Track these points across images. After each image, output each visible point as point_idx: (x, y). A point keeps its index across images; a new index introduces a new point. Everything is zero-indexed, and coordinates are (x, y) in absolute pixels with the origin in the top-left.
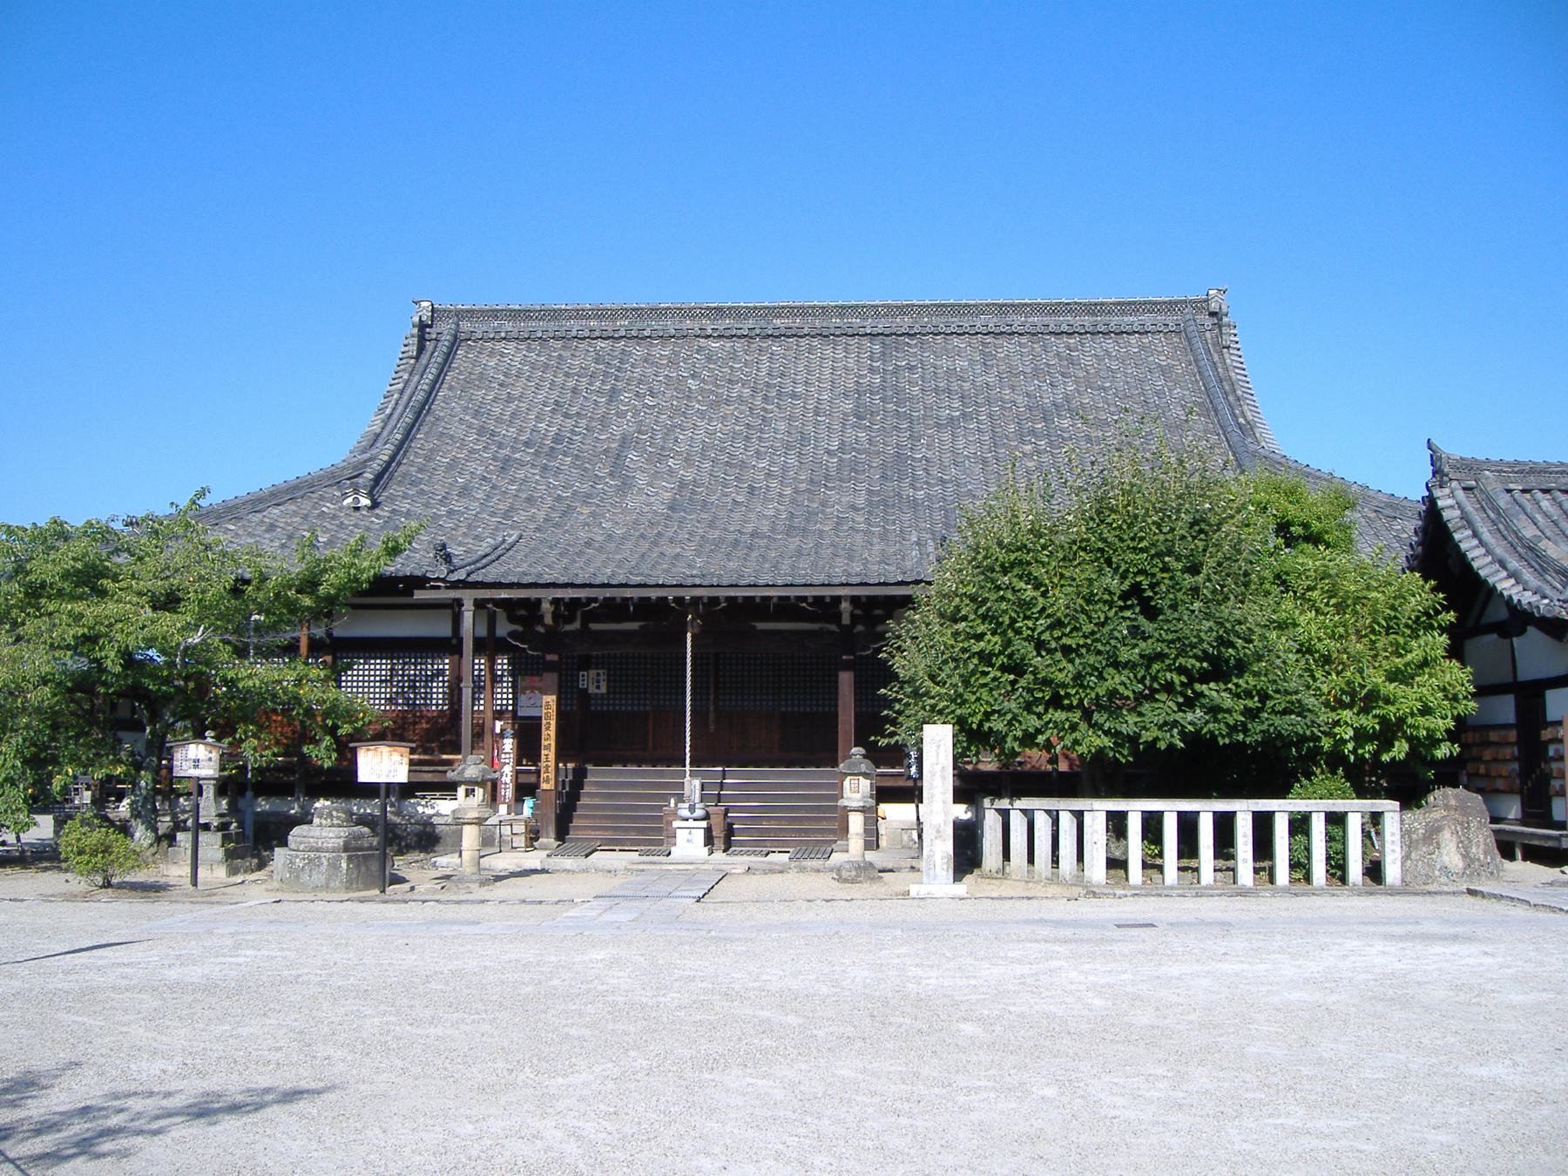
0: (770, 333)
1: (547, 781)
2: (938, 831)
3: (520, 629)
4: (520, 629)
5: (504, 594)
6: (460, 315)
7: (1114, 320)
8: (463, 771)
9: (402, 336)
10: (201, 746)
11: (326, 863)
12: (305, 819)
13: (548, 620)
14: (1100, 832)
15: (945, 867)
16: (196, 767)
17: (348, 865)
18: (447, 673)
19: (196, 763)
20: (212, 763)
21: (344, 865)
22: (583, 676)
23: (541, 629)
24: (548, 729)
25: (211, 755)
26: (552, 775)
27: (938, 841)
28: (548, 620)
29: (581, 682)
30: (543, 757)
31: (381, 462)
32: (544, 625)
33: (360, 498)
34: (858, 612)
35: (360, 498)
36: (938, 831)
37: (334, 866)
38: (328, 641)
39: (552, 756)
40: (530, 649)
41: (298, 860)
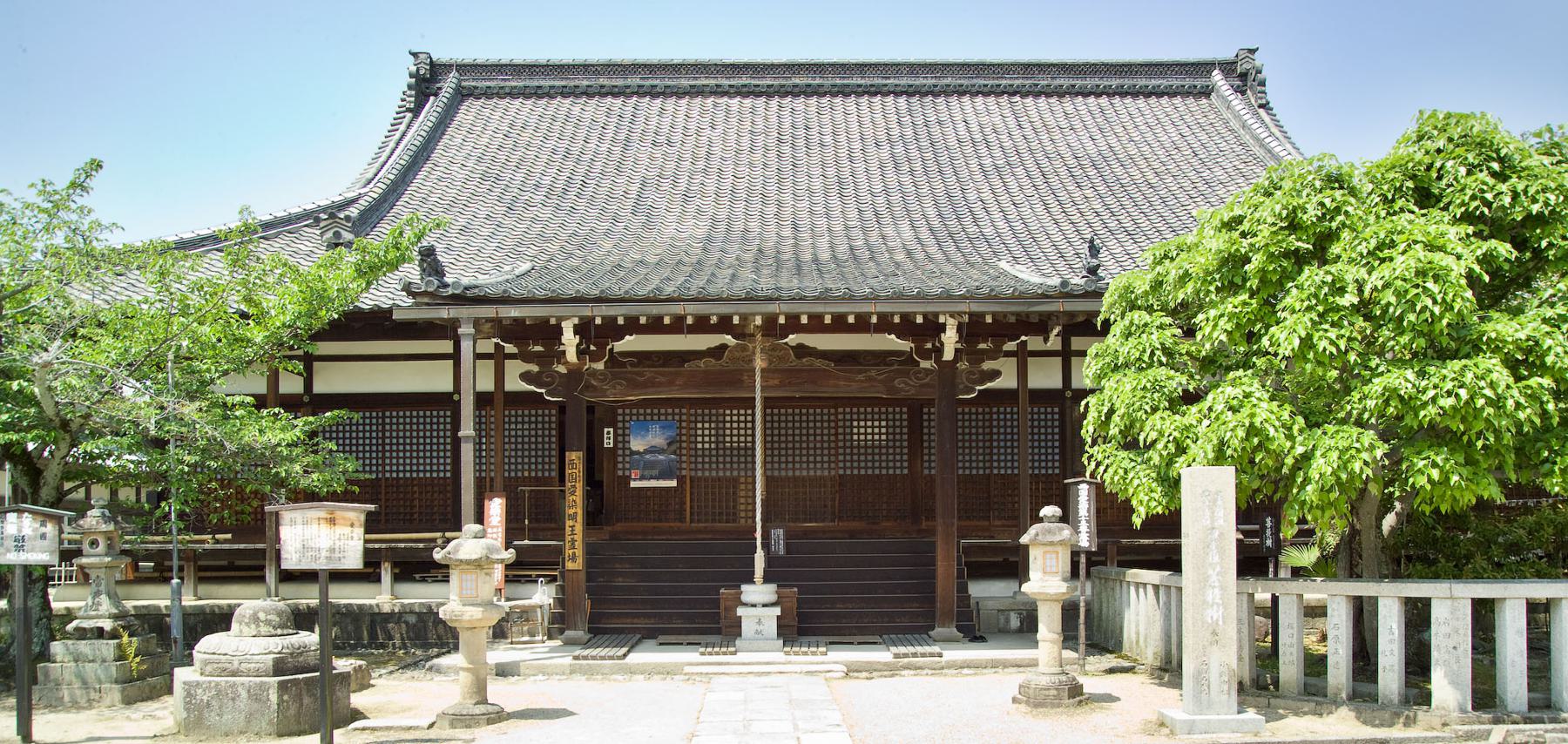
0: (789, 90)
1: (573, 558)
2: (1214, 633)
3: (535, 368)
4: (535, 368)
5: (514, 312)
6: (463, 68)
7: (1141, 82)
8: (456, 550)
9: (397, 84)
10: (27, 516)
11: (244, 694)
12: (220, 621)
13: (571, 356)
14: (1461, 631)
15: (1226, 687)
16: (19, 548)
17: (280, 697)
18: (449, 488)
19: (20, 543)
20: (45, 543)
21: (274, 697)
22: (608, 433)
23: (562, 369)
24: (573, 493)
25: (43, 530)
26: (579, 552)
27: (1215, 648)
28: (571, 356)
29: (606, 441)
30: (568, 530)
31: (370, 200)
32: (566, 363)
33: (343, 232)
34: (397, 571)
35: (343, 232)
36: (1214, 633)
37: (257, 695)
38: (306, 399)
39: (579, 528)
40: (548, 393)
41: (199, 691)
